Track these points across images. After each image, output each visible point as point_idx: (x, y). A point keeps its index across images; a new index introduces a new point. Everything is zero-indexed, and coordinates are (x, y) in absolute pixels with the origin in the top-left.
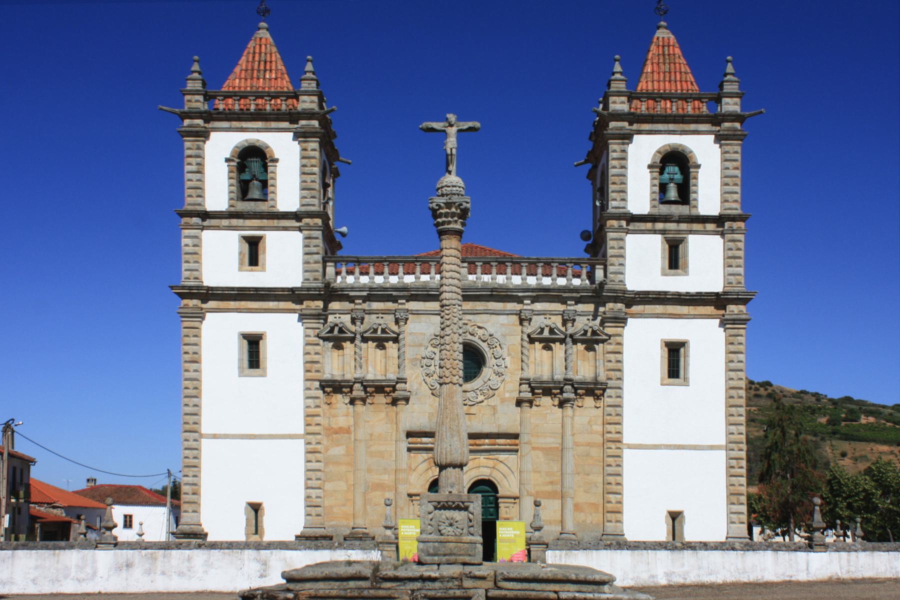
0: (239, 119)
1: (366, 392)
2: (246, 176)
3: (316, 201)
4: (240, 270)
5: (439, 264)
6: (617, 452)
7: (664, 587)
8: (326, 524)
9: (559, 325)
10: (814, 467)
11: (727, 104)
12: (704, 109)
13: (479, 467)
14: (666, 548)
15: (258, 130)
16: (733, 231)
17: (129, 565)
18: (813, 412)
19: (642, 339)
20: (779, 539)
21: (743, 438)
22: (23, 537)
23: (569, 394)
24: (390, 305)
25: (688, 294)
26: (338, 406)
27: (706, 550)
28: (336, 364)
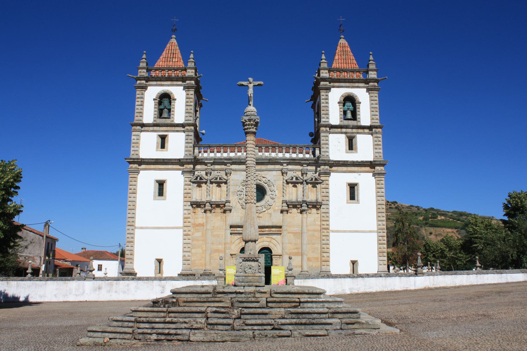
0: (161, 81)
1: (212, 207)
2: (162, 107)
3: (191, 119)
4: (157, 150)
5: (246, 148)
6: (327, 234)
7: (349, 294)
8: (192, 269)
9: (300, 176)
10: (418, 239)
11: (371, 74)
12: (361, 77)
13: (264, 242)
14: (350, 277)
15: (168, 85)
16: (376, 133)
17: (100, 288)
18: (416, 215)
19: (338, 182)
20: (402, 271)
21: (385, 227)
22: (51, 275)
23: (305, 207)
24: (223, 167)
25: (357, 162)
26: (199, 213)
27: (368, 277)
28: (199, 194)
